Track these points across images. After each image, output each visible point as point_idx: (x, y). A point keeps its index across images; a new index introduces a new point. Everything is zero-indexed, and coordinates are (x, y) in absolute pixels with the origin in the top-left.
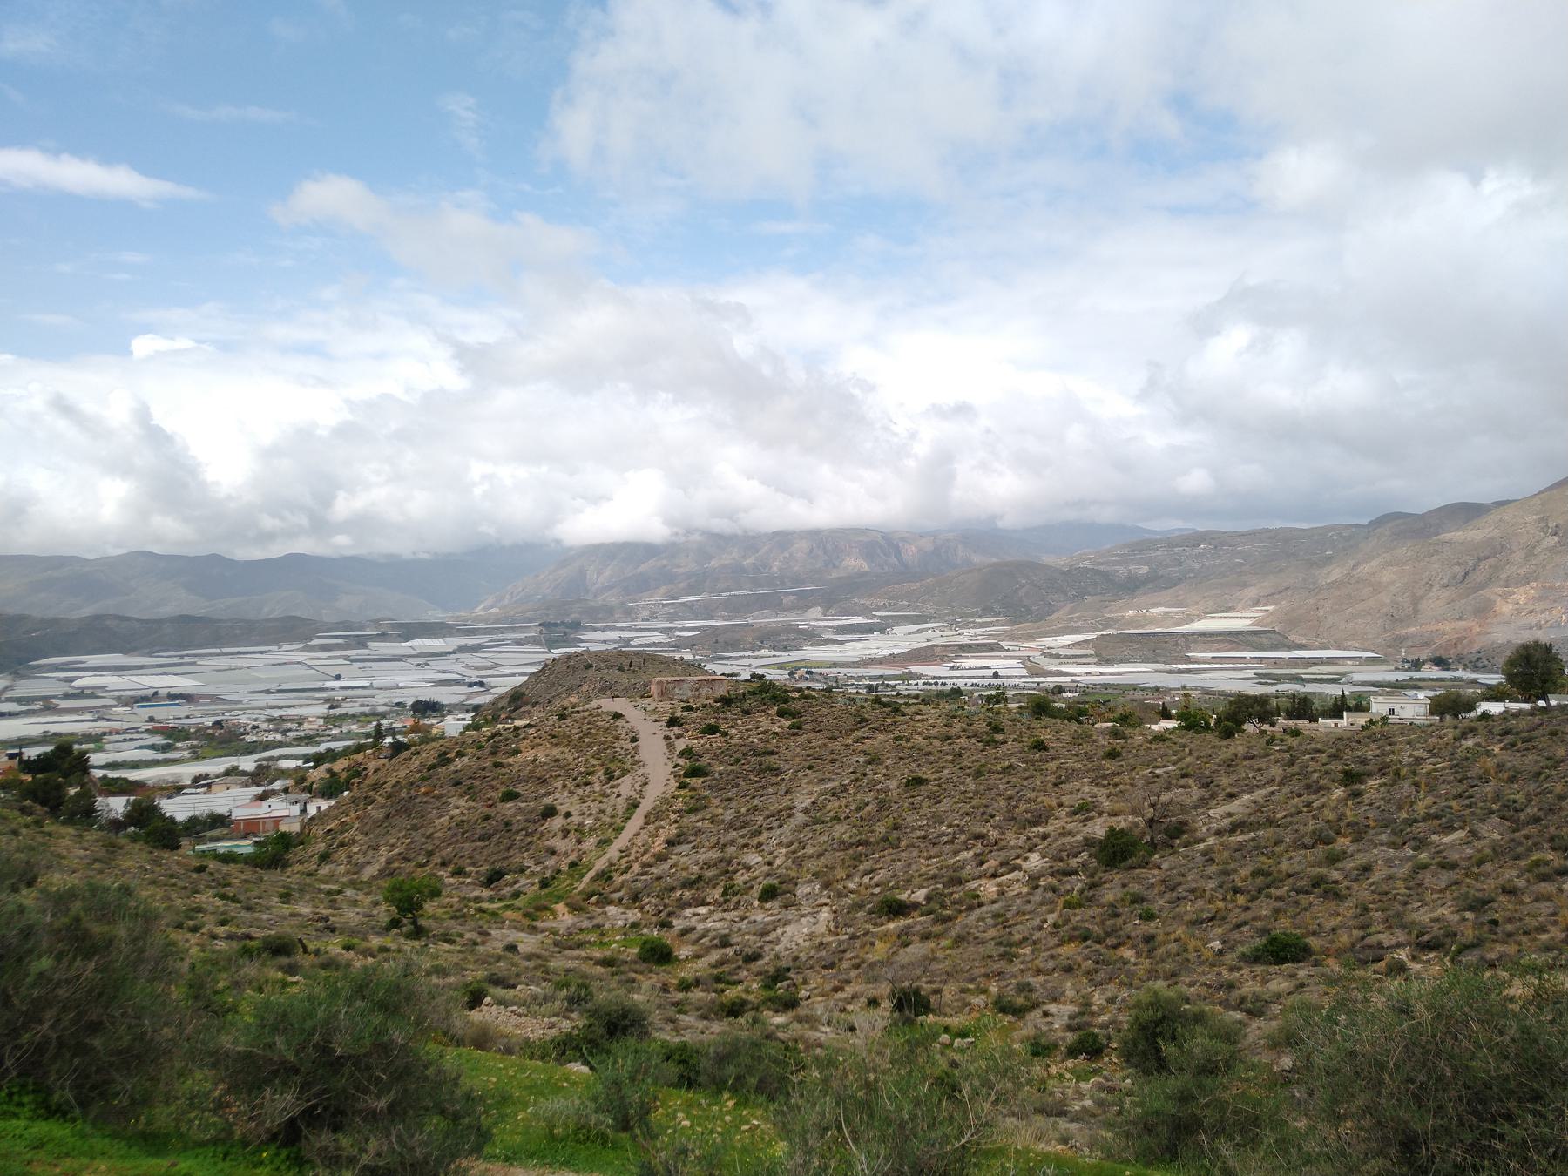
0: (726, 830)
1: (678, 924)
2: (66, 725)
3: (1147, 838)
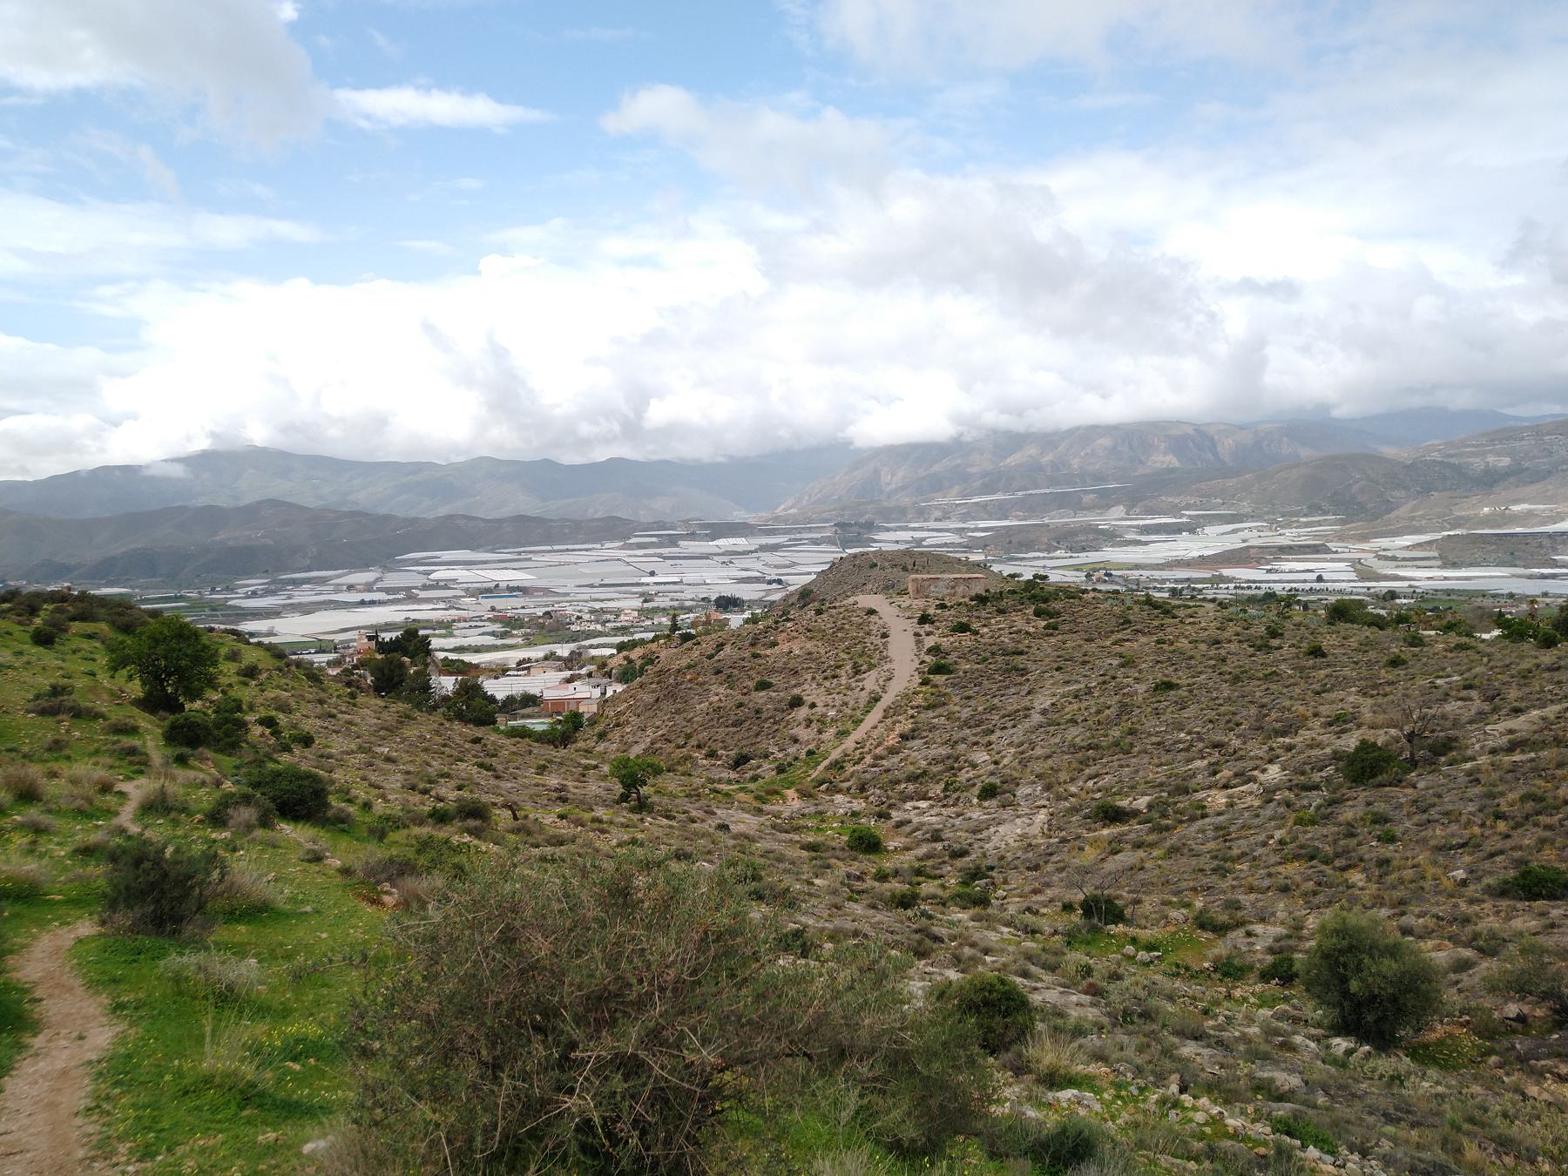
0: (961, 728)
1: (896, 815)
2: (423, 613)
3: (1407, 754)
